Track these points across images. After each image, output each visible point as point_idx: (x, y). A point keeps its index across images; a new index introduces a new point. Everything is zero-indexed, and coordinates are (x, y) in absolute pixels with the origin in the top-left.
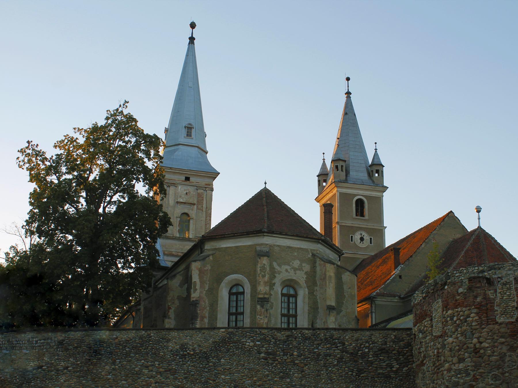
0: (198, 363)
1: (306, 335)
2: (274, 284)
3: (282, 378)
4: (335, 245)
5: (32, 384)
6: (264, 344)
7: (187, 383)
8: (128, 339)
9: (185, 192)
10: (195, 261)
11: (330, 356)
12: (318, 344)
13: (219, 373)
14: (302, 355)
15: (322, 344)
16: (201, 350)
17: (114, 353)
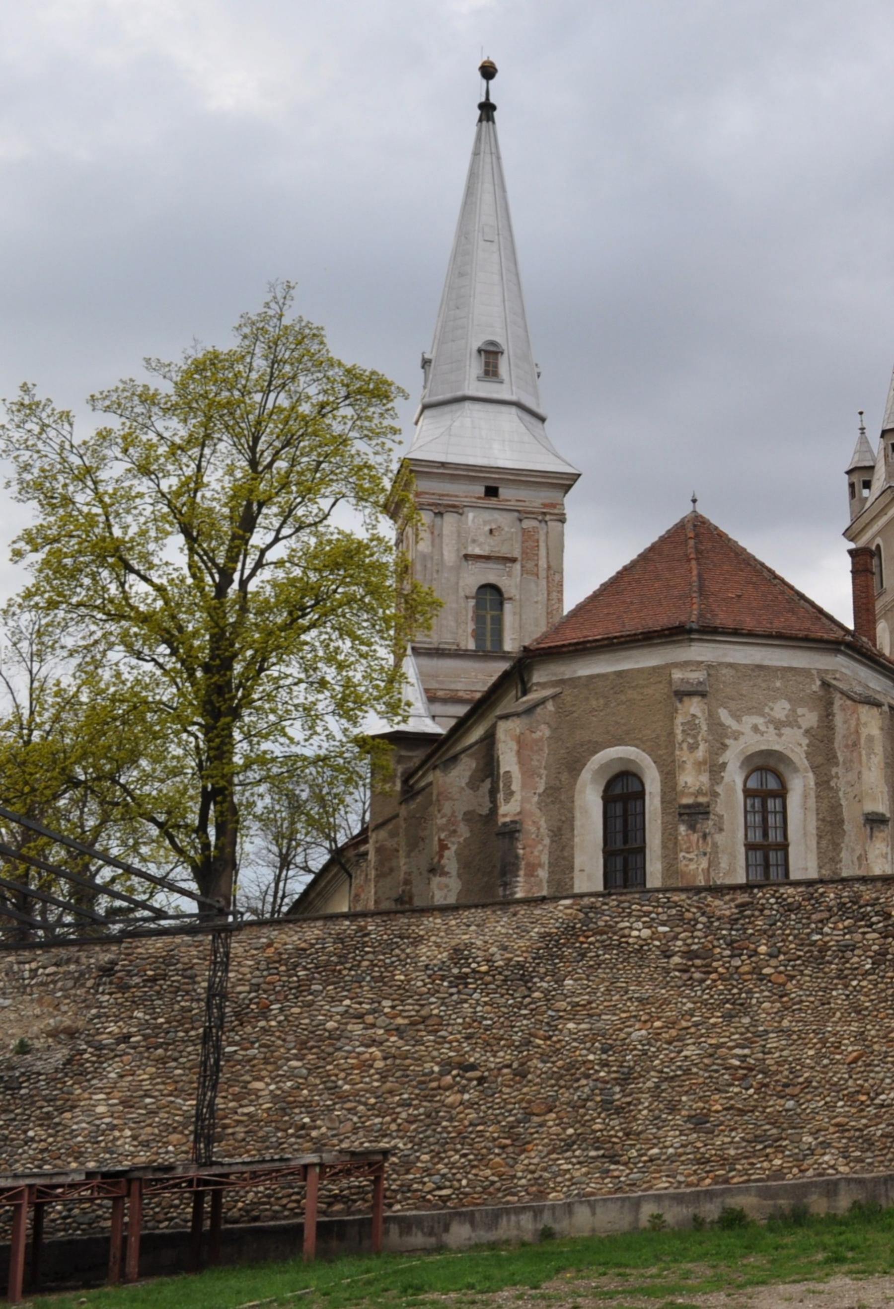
0: (502, 996)
1: (790, 900)
2: (724, 765)
3: (728, 1017)
4: (883, 655)
5: (23, 1092)
6: (679, 929)
7: (473, 1050)
8: (303, 945)
9: (487, 528)
10: (506, 717)
11: (852, 951)
12: (821, 921)
13: (561, 1017)
14: (780, 952)
15: (832, 920)
16: (510, 960)
17: (264, 986)
